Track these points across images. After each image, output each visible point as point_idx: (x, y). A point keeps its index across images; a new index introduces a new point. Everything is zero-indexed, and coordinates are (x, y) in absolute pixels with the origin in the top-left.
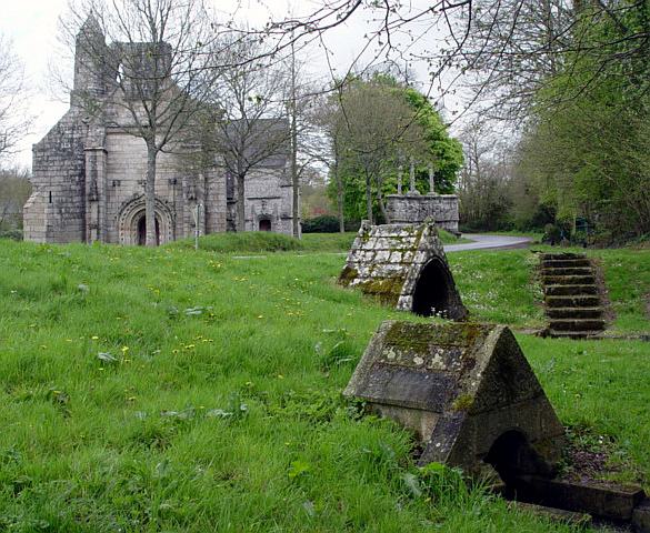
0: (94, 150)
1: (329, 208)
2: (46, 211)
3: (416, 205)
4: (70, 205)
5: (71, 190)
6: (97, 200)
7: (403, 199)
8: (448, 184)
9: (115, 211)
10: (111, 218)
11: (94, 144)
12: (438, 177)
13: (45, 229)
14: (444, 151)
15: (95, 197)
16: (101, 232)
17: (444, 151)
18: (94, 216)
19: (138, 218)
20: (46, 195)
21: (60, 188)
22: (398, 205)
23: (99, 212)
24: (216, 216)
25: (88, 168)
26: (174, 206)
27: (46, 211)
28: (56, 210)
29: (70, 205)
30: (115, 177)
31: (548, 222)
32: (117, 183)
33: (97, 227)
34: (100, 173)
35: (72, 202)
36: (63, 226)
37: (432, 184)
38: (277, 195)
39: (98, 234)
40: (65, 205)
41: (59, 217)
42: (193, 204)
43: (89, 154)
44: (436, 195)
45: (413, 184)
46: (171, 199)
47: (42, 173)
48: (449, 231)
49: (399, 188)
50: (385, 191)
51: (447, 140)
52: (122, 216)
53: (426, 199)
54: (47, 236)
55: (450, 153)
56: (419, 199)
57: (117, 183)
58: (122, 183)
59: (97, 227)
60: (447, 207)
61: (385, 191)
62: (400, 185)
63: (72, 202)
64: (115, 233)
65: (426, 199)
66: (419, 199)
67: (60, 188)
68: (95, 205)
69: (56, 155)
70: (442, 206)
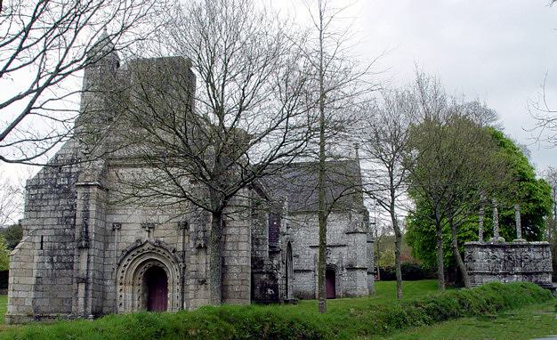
0: (87, 186)
1: (409, 255)
2: (36, 260)
3: (500, 254)
4: (62, 253)
5: (64, 235)
6: (87, 247)
7: (485, 247)
8: (536, 230)
9: (113, 261)
10: (108, 269)
11: (88, 179)
12: (525, 220)
13: (33, 281)
14: (531, 192)
15: (83, 243)
16: (90, 287)
17: (531, 192)
18: (84, 266)
19: (142, 270)
20: (37, 240)
21: (53, 232)
22: (479, 254)
23: (88, 262)
24: (235, 270)
25: (80, 208)
26: (183, 257)
27: (36, 259)
28: (47, 259)
29: (62, 253)
30: (116, 219)
31: (426, 231)
32: (118, 226)
33: (85, 281)
34: (93, 214)
35: (65, 249)
36: (53, 278)
37: (519, 230)
38: (343, 242)
39: (86, 289)
40: (57, 253)
41: (50, 267)
42: (202, 253)
43: (80, 191)
44: (525, 242)
45: (496, 230)
46: (180, 248)
47: (33, 214)
48: (541, 284)
49: (481, 235)
50: (465, 238)
51: (534, 181)
52: (122, 268)
53: (513, 246)
54: (36, 290)
55: (539, 195)
56: (504, 247)
57: (118, 227)
58: (123, 227)
59: (85, 281)
60: (538, 256)
61: (465, 238)
62: (481, 230)
63: (65, 249)
64: (112, 288)
65: (513, 246)
66: (504, 247)
67: (53, 232)
68: (85, 254)
69: (51, 192)
70: (532, 255)
